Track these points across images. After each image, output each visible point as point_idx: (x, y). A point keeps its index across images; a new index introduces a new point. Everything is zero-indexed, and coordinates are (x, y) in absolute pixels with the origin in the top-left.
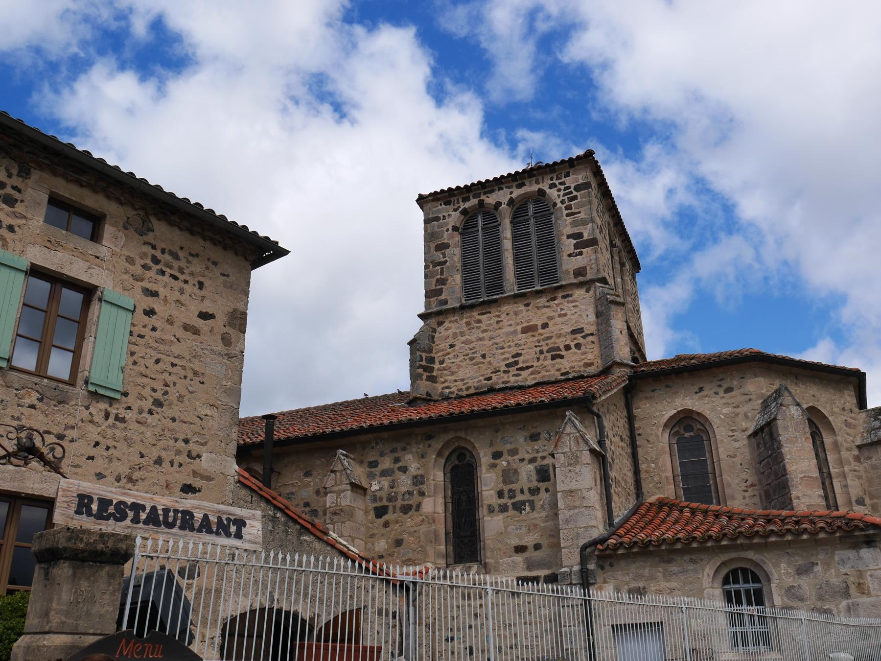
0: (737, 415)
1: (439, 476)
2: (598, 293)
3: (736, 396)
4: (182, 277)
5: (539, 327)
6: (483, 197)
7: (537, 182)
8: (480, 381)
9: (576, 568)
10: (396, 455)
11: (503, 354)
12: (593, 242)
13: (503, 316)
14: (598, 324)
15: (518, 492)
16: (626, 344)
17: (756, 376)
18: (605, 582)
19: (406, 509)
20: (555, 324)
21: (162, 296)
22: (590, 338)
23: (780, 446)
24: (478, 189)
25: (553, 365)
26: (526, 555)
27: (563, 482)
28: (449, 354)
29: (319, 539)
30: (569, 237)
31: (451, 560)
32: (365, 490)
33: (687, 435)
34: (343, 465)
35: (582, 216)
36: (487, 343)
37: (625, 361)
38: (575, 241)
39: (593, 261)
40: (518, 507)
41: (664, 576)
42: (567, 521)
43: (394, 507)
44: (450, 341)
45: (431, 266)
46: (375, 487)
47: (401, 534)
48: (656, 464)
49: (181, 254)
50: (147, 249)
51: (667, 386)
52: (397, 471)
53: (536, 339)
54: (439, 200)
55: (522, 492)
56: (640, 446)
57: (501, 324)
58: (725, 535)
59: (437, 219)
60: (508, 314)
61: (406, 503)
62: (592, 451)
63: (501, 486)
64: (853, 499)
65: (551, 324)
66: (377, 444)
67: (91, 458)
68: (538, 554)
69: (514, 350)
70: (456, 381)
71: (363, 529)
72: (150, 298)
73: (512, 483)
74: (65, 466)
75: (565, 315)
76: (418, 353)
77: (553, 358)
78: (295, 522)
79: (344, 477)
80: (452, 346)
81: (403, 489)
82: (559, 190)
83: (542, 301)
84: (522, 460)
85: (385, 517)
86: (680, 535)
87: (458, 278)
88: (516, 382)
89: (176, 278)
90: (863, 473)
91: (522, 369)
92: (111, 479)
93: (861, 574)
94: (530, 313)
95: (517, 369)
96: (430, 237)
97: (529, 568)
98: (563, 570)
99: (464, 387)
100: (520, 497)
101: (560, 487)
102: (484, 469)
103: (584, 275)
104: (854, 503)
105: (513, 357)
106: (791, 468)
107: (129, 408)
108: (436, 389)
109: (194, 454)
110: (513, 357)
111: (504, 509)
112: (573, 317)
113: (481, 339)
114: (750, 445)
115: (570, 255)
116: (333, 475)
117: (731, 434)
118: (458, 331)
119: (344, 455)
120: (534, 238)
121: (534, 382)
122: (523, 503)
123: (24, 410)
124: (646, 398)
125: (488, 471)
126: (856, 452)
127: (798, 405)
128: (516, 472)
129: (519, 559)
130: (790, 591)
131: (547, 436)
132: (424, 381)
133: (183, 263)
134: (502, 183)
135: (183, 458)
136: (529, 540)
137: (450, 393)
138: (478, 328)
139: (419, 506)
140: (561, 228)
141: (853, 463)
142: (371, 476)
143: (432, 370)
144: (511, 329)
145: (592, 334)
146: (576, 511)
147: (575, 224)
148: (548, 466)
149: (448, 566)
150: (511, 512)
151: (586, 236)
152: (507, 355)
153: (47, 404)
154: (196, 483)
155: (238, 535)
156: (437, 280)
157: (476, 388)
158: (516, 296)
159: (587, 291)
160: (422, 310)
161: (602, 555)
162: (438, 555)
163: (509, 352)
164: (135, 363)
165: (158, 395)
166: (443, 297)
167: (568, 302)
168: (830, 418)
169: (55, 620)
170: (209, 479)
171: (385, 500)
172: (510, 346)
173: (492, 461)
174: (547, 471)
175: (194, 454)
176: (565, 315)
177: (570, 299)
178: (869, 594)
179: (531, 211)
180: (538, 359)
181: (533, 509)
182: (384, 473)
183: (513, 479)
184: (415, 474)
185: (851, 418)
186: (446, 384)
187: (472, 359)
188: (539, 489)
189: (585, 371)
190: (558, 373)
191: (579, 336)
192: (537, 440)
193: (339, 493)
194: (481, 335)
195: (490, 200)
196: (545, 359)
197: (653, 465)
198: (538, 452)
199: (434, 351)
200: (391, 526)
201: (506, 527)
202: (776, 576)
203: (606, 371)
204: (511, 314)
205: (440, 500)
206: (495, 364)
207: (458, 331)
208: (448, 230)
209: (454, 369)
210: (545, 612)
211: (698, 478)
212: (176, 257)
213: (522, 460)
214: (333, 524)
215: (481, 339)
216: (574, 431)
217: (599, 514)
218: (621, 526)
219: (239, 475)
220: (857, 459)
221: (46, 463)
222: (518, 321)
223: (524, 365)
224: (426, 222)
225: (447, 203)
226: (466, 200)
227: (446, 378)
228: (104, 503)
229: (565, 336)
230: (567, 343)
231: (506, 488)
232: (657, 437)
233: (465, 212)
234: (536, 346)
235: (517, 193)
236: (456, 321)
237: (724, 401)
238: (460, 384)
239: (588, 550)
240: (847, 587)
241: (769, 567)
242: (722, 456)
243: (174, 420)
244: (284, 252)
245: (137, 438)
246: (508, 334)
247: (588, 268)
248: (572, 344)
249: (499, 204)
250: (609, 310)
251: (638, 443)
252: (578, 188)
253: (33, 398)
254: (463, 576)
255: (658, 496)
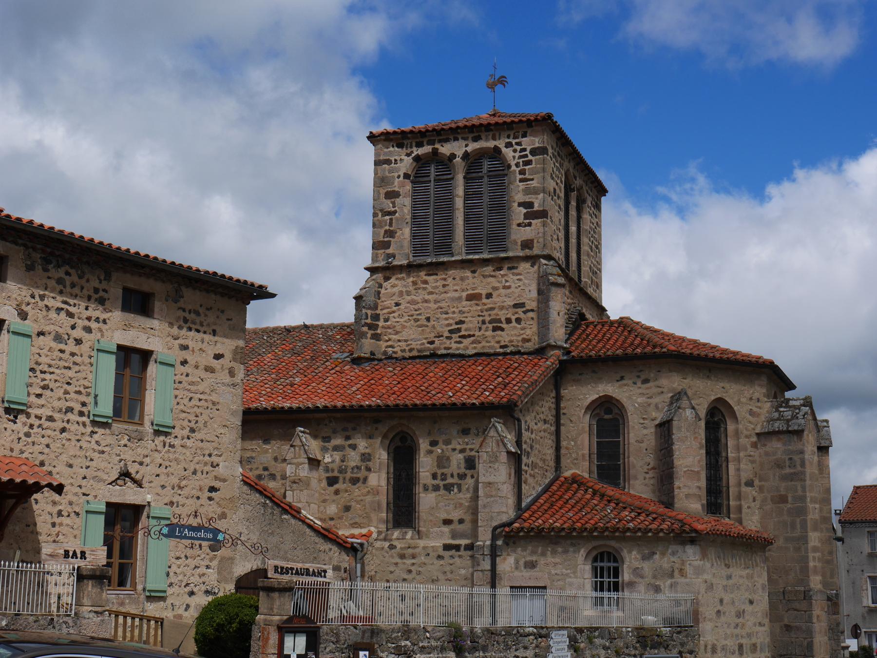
0: (649, 405)
1: (384, 455)
2: (541, 270)
3: (651, 388)
4: (202, 329)
5: (484, 296)
6: (437, 146)
7: (494, 139)
8: (423, 344)
9: (488, 543)
10: (348, 434)
11: (446, 319)
12: (543, 214)
13: (450, 280)
14: (539, 302)
15: (449, 476)
16: (562, 326)
17: (670, 371)
18: (508, 555)
19: (354, 481)
20: (499, 295)
21: (191, 348)
22: (531, 314)
23: (672, 444)
24: (433, 136)
25: (494, 337)
26: (452, 527)
27: (484, 473)
28: (394, 312)
29: (294, 517)
30: (520, 205)
31: (390, 525)
32: (319, 461)
33: (607, 417)
34: (301, 441)
35: (534, 184)
36: (432, 305)
37: (559, 343)
38: (525, 211)
39: (541, 235)
40: (448, 488)
41: (552, 553)
42: (485, 506)
43: (344, 479)
44: (396, 299)
45: (380, 214)
46: (328, 459)
47: (349, 502)
48: (576, 443)
49: (201, 310)
50: (181, 313)
51: (594, 372)
52: (347, 448)
53: (479, 308)
54: (391, 140)
55: (452, 476)
56: (563, 425)
57: (447, 288)
58: (596, 528)
59: (388, 162)
60: (454, 279)
61: (355, 475)
62: (509, 453)
63: (435, 469)
64: (743, 481)
65: (495, 294)
66: (330, 421)
67: (158, 475)
68: (461, 526)
69: (458, 317)
70: (399, 341)
71: (317, 495)
72: (184, 352)
73: (445, 467)
74: (145, 484)
75: (509, 287)
76: (364, 311)
77: (495, 329)
78: (278, 505)
79: (302, 452)
80: (397, 304)
81: (353, 464)
82: (515, 151)
83: (489, 270)
84: (454, 450)
85: (336, 486)
86: (565, 526)
87: (407, 231)
88: (458, 349)
89: (198, 331)
90: (757, 458)
91: (464, 337)
92: (169, 488)
93: (683, 563)
94: (475, 280)
95: (460, 337)
96: (380, 181)
97: (454, 537)
98: (478, 543)
99: (407, 348)
100: (450, 480)
101: (482, 479)
102: (422, 452)
103: (531, 248)
104: (743, 485)
105: (457, 323)
106: (677, 462)
107: (176, 437)
108: (379, 347)
109: (215, 464)
110: (457, 323)
111: (436, 488)
112: (517, 291)
113: (426, 301)
114: (656, 433)
115: (519, 225)
116: (292, 449)
117: (642, 421)
118: (404, 290)
119: (302, 432)
120: (486, 199)
121: (474, 352)
122: (452, 485)
123: (121, 448)
124: (574, 380)
125: (425, 455)
126: (754, 439)
127: (693, 408)
128: (448, 459)
129: (446, 529)
130: (636, 571)
131: (476, 432)
132: (369, 340)
133: (202, 318)
134: (458, 133)
135: (208, 468)
136: (455, 515)
137: (394, 352)
138: (425, 289)
139: (365, 479)
140: (513, 194)
141: (750, 449)
142: (324, 450)
143: (376, 327)
144: (456, 295)
145: (532, 310)
146: (492, 499)
147: (527, 191)
148: (474, 457)
149: (387, 530)
150: (442, 492)
151: (536, 207)
152: (451, 321)
153: (133, 443)
154: (217, 484)
155: (325, 577)
156: (386, 231)
157: (419, 351)
158: (463, 262)
159: (532, 266)
160: (368, 262)
161: (509, 536)
162: (380, 521)
163: (453, 318)
164: (178, 403)
165: (192, 425)
166: (390, 251)
167: (513, 274)
168: (735, 408)
169: (275, 611)
170: (224, 480)
171: (336, 472)
172: (454, 313)
173: (429, 448)
174: (474, 461)
175: (215, 464)
176: (509, 287)
177: (515, 271)
178: (686, 577)
179: (485, 169)
180: (480, 329)
181: (460, 491)
182: (336, 448)
183: (446, 465)
184: (363, 451)
185: (757, 407)
186: (390, 343)
187: (416, 320)
188: (466, 475)
189: (522, 347)
190: (498, 345)
191: (520, 310)
192: (467, 434)
193: (298, 465)
194: (427, 297)
195: (446, 149)
196: (486, 331)
197: (573, 443)
198: (467, 444)
199: (380, 308)
200: (341, 494)
201: (437, 504)
202: (628, 559)
203: (541, 351)
204: (458, 278)
205: (384, 476)
206: (439, 329)
207: (404, 290)
208: (399, 177)
209: (398, 328)
210: (463, 572)
211: (610, 462)
212: (198, 313)
213: (454, 450)
214: (293, 491)
215: (426, 301)
216: (496, 435)
217: (511, 501)
218: (528, 508)
219: (242, 475)
220: (754, 445)
221: (134, 481)
222: (464, 287)
223: (466, 333)
224: (377, 163)
225: (400, 146)
226: (419, 145)
227: (391, 336)
228: (282, 568)
229: (507, 309)
230: (508, 316)
231: (439, 472)
232: (579, 417)
233: (417, 159)
234: (479, 316)
235: (472, 146)
236: (403, 279)
237: (640, 391)
238: (403, 344)
239: (499, 530)
240: (673, 571)
241: (625, 553)
242: (632, 441)
243: (202, 441)
244: (273, 296)
245: (181, 458)
246: (453, 299)
247: (535, 241)
248: (513, 318)
249: (453, 156)
250: (549, 291)
251: (562, 422)
252: (534, 152)
253: (125, 441)
254: (402, 538)
255: (573, 471)
